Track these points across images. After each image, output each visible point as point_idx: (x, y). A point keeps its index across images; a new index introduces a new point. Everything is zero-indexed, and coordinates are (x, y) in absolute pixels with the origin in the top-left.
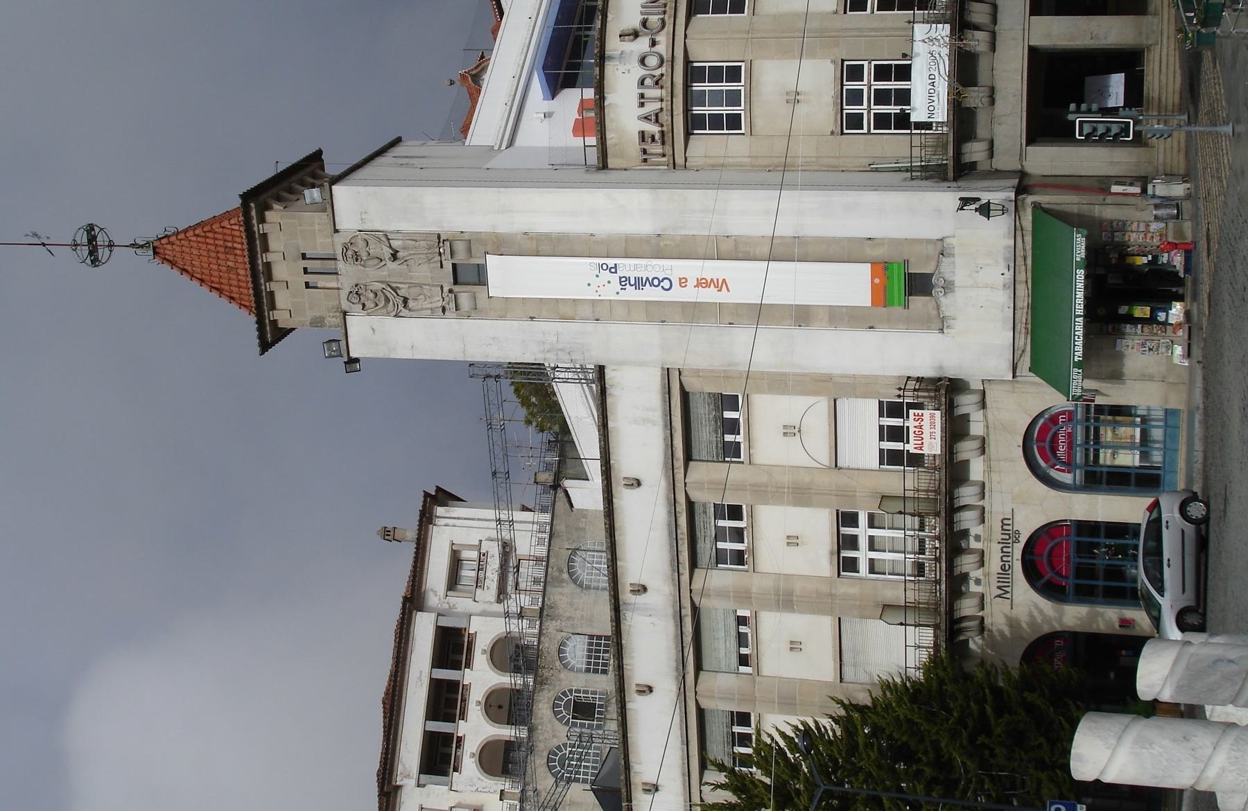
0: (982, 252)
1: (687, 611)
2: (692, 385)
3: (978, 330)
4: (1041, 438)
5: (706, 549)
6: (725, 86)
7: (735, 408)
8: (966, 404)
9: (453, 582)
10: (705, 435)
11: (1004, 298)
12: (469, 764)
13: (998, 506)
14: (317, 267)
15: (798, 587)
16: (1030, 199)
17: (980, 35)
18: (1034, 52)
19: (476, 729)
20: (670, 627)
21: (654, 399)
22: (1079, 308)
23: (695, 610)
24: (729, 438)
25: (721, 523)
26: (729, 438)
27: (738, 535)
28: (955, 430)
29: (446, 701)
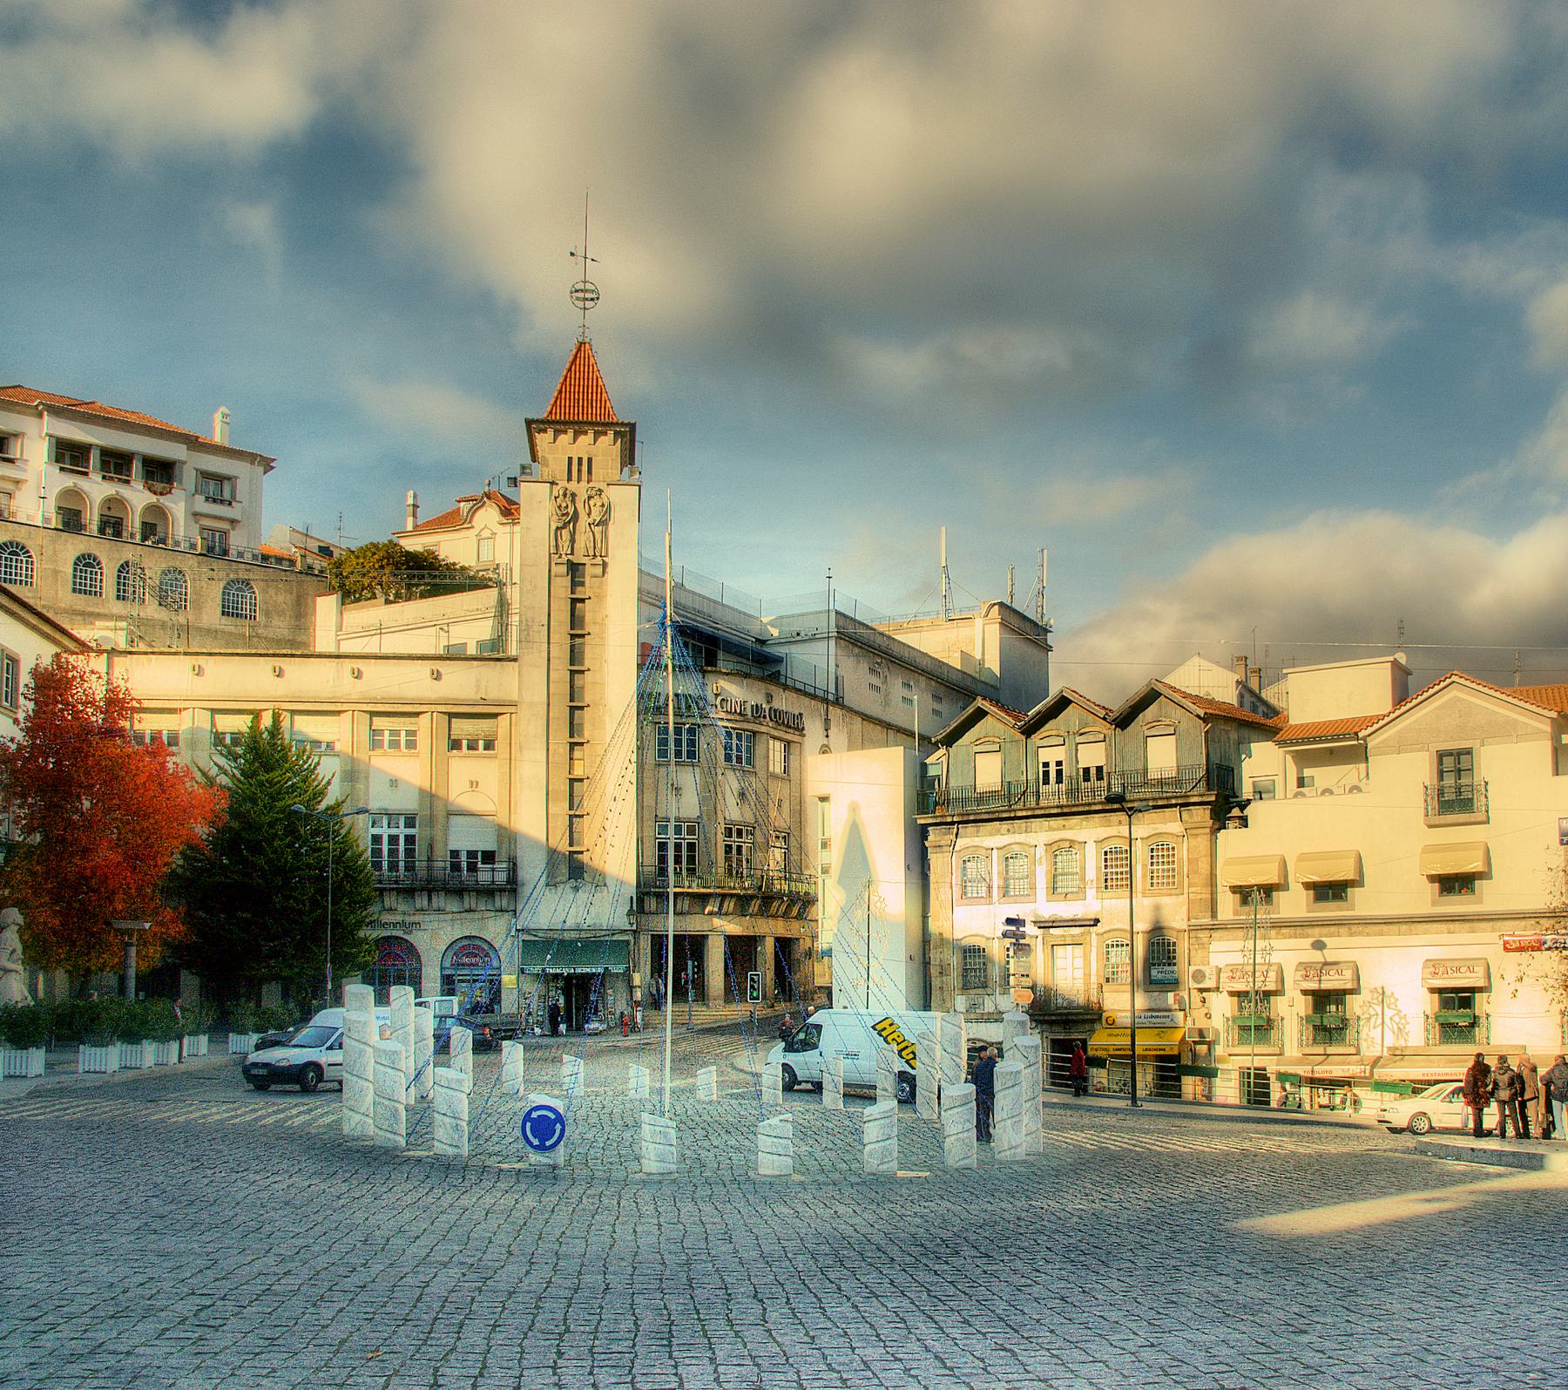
0: (604, 911)
1: (339, 707)
2: (503, 721)
3: (553, 910)
4: (479, 948)
5: (379, 723)
6: (684, 748)
7: (469, 748)
8: (502, 901)
9: (206, 475)
10: (463, 728)
11: (570, 923)
12: (70, 481)
13: (429, 920)
14: (580, 468)
15: (361, 786)
16: (631, 938)
17: (426, 903)
18: (705, 937)
19: (96, 489)
20: (326, 694)
21: (493, 694)
22: (579, 971)
23: (339, 713)
24: (481, 743)
25: (403, 734)
26: (481, 743)
27: (395, 744)
28: (489, 892)
29: (116, 463)
